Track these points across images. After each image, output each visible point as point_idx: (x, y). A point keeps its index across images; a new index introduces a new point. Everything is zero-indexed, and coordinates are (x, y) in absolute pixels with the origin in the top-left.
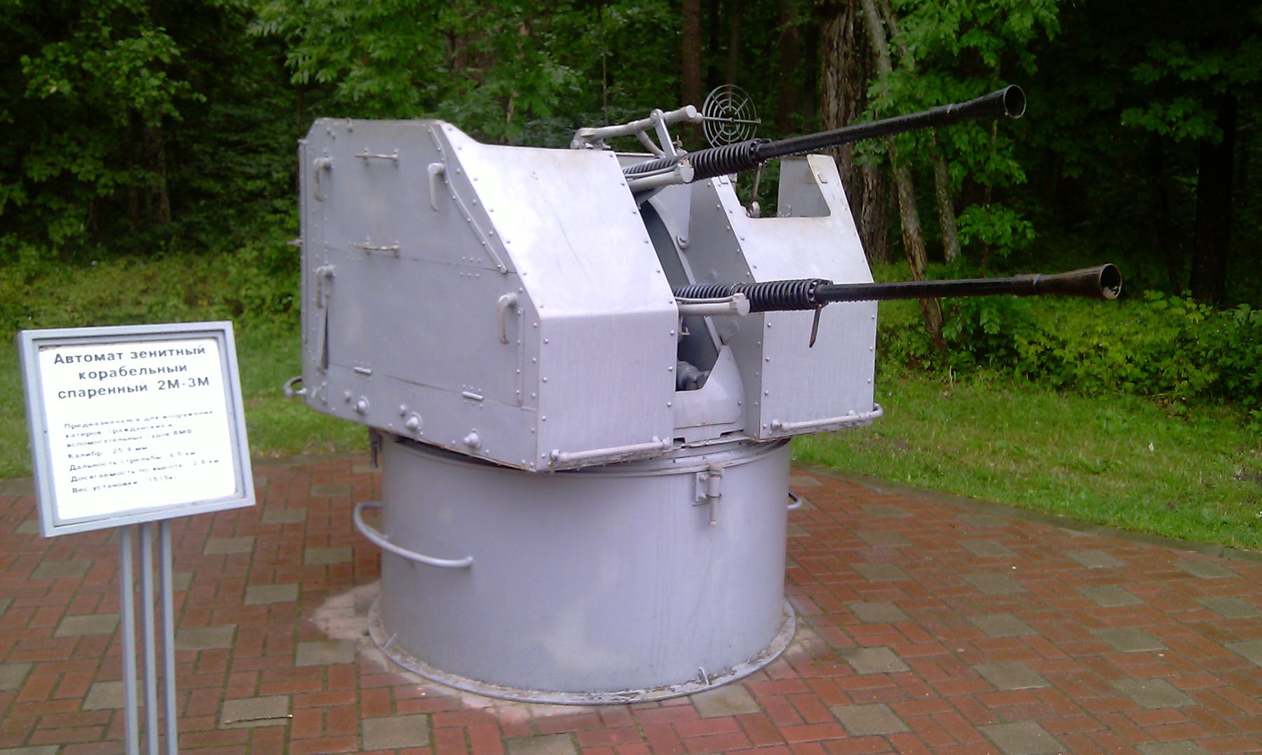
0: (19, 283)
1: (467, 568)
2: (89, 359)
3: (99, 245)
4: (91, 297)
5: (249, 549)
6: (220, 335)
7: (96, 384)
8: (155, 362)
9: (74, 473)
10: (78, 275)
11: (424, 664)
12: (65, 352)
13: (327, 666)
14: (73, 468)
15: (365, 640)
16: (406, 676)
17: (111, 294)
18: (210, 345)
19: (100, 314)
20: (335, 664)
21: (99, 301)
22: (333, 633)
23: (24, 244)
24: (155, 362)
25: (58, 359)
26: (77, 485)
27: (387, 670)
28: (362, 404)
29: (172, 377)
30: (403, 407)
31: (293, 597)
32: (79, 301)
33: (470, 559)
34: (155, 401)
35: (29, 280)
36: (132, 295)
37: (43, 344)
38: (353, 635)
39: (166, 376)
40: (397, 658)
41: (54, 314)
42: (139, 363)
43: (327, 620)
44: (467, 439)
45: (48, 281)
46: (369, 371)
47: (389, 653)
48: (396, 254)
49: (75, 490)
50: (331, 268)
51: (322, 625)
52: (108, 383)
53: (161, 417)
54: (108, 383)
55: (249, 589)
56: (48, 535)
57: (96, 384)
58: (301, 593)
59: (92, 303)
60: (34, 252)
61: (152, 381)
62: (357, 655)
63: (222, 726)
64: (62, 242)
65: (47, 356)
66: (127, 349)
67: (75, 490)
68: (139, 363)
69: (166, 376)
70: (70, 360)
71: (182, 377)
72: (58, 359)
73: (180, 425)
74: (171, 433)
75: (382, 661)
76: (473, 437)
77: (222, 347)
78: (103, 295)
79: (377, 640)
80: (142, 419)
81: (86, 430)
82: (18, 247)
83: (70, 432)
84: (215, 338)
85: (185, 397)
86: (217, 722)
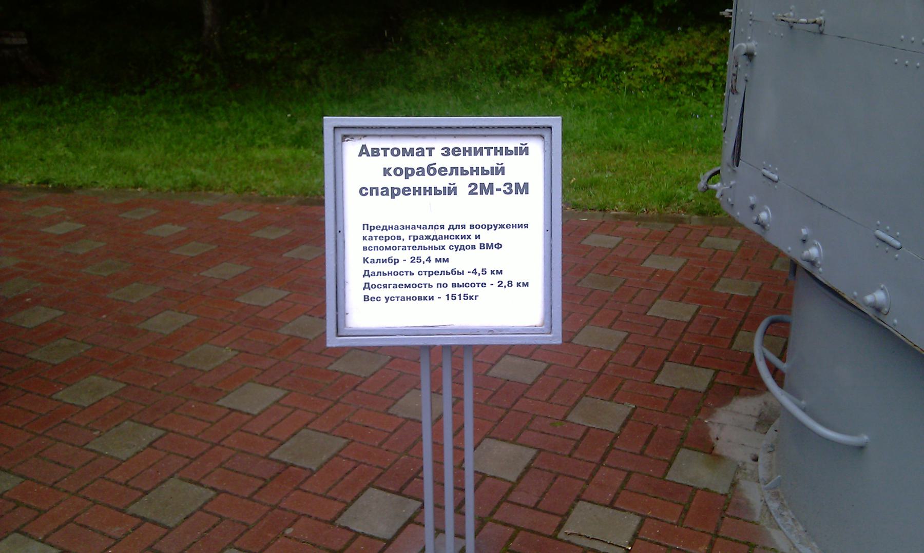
0: (625, 44)
1: (861, 448)
2: (396, 152)
3: (689, 14)
4: (672, 56)
5: (688, 318)
6: (546, 134)
7: (400, 182)
8: (466, 162)
9: (367, 279)
10: (668, 39)
11: (801, 528)
12: (371, 144)
13: (695, 490)
14: (367, 274)
15: (750, 466)
16: (775, 534)
17: (688, 56)
18: (536, 146)
19: (677, 71)
20: (706, 490)
21: (677, 61)
22: (721, 448)
23: (635, 13)
24: (466, 162)
25: (363, 151)
26: (372, 293)
27: (757, 519)
28: (763, 216)
29: (486, 180)
30: (804, 231)
31: (702, 386)
32: (663, 60)
33: (866, 438)
34: (463, 208)
35: (633, 42)
36: (703, 55)
37: (348, 134)
38: (740, 455)
39: (478, 179)
40: (774, 506)
41: (642, 70)
42: (450, 162)
43: (722, 425)
44: (869, 298)
45: (646, 43)
46: (775, 177)
47: (767, 496)
48: (819, 28)
49: (366, 298)
50: (752, 45)
51: (715, 432)
52: (415, 181)
53: (468, 227)
54: (415, 181)
55: (667, 364)
56: (328, 345)
57: (400, 182)
58: (712, 383)
59: (672, 62)
60: (640, 19)
61: (462, 182)
62: (734, 485)
63: (561, 535)
64: (661, 11)
65: (351, 148)
66: (438, 144)
67: (366, 298)
68: (450, 162)
69: (478, 179)
70: (375, 152)
71: (498, 181)
72: (363, 151)
73: (488, 237)
74: (478, 247)
75: (757, 506)
76: (879, 296)
77: (548, 148)
78: (681, 55)
79: (762, 473)
80: (447, 227)
81: (384, 233)
82: (631, 15)
83: (367, 233)
84: (542, 137)
85: (496, 208)
86: (560, 527)
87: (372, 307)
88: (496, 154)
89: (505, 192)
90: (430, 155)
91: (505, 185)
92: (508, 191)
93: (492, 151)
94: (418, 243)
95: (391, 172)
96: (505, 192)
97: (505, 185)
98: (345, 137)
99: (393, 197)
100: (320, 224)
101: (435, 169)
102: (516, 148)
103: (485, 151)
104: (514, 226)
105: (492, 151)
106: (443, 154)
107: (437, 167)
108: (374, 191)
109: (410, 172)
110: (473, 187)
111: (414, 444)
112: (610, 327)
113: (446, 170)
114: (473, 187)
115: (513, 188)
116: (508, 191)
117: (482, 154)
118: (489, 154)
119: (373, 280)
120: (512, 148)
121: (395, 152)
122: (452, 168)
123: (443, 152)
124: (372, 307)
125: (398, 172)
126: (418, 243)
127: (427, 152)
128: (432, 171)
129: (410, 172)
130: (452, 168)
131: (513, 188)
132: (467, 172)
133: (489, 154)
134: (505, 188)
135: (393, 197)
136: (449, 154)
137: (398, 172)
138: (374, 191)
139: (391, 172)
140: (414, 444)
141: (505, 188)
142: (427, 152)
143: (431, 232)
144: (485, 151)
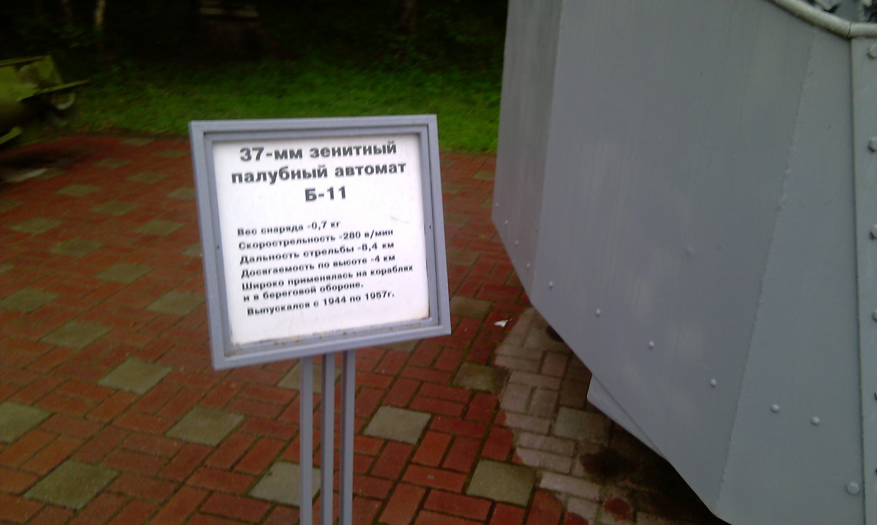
9: (245, 266)
14: (245, 274)
49: (250, 312)
67: (250, 312)
84: (418, 135)
87: (257, 320)
88: (365, 153)
90: (402, 170)
93: (361, 151)
94: (300, 287)
98: (215, 143)
100: (197, 266)
102: (384, 147)
103: (354, 151)
105: (361, 151)
106: (312, 156)
107: (289, 170)
108: (237, 178)
111: (292, 400)
117: (351, 154)
118: (358, 153)
119: (251, 267)
120: (380, 146)
121: (369, 170)
123: (313, 153)
124: (257, 320)
126: (300, 287)
127: (399, 169)
128: (284, 175)
133: (358, 153)
136: (317, 155)
138: (237, 178)
140: (292, 400)
142: (399, 169)
143: (287, 236)
144: (354, 151)
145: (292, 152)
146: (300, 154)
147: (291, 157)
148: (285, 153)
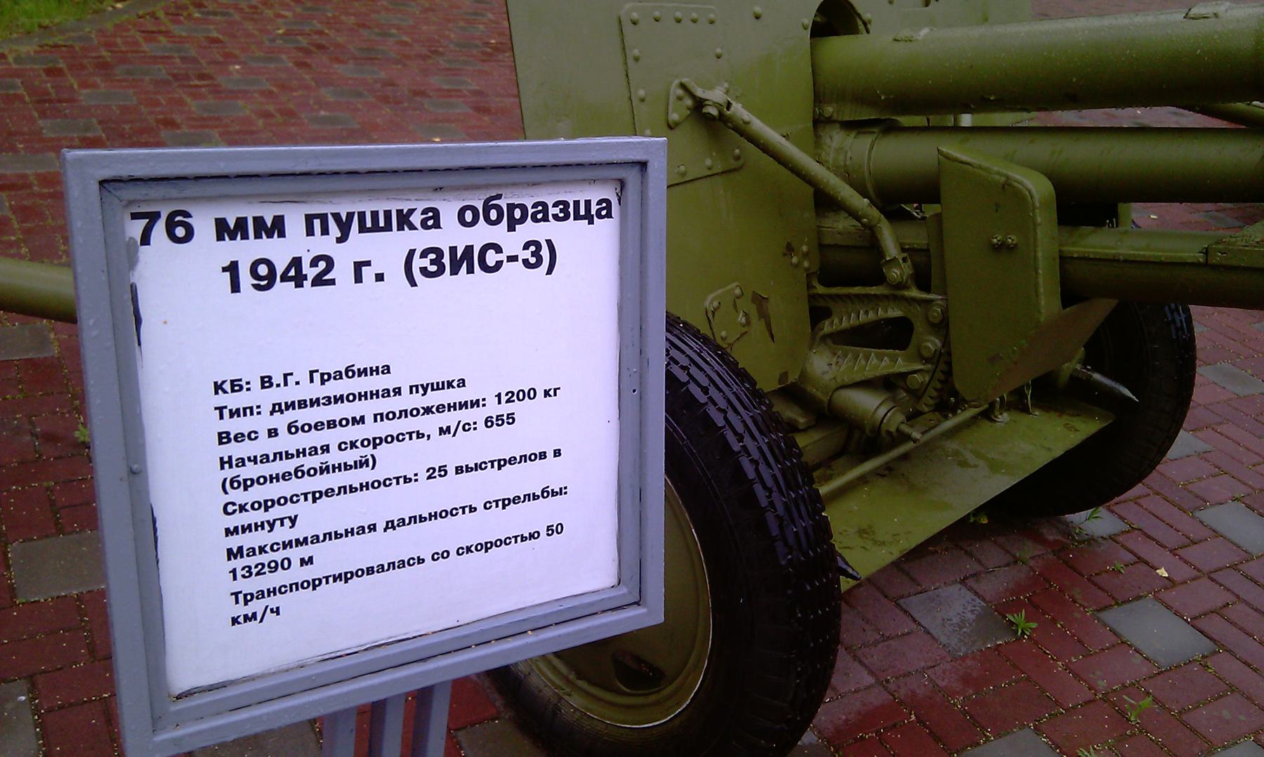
6: (632, 176)
14: (224, 438)
89: (526, 262)
91: (526, 247)
92: (533, 260)
95: (358, 444)
96: (526, 262)
97: (526, 247)
99: (314, 589)
101: (499, 208)
104: (524, 458)
107: (355, 369)
108: (317, 223)
109: (517, 214)
110: (322, 265)
112: (672, 323)
113: (333, 490)
114: (322, 265)
115: (446, 260)
116: (533, 260)
119: (235, 450)
122: (340, 488)
125: (256, 506)
128: (350, 374)
129: (517, 214)
130: (340, 488)
131: (446, 260)
132: (293, 456)
134: (527, 254)
135: (314, 589)
137: (256, 506)
138: (317, 223)
139: (358, 444)
141: (527, 254)
145: (259, 221)
146: (278, 227)
147: (400, 228)
148: (241, 223)
